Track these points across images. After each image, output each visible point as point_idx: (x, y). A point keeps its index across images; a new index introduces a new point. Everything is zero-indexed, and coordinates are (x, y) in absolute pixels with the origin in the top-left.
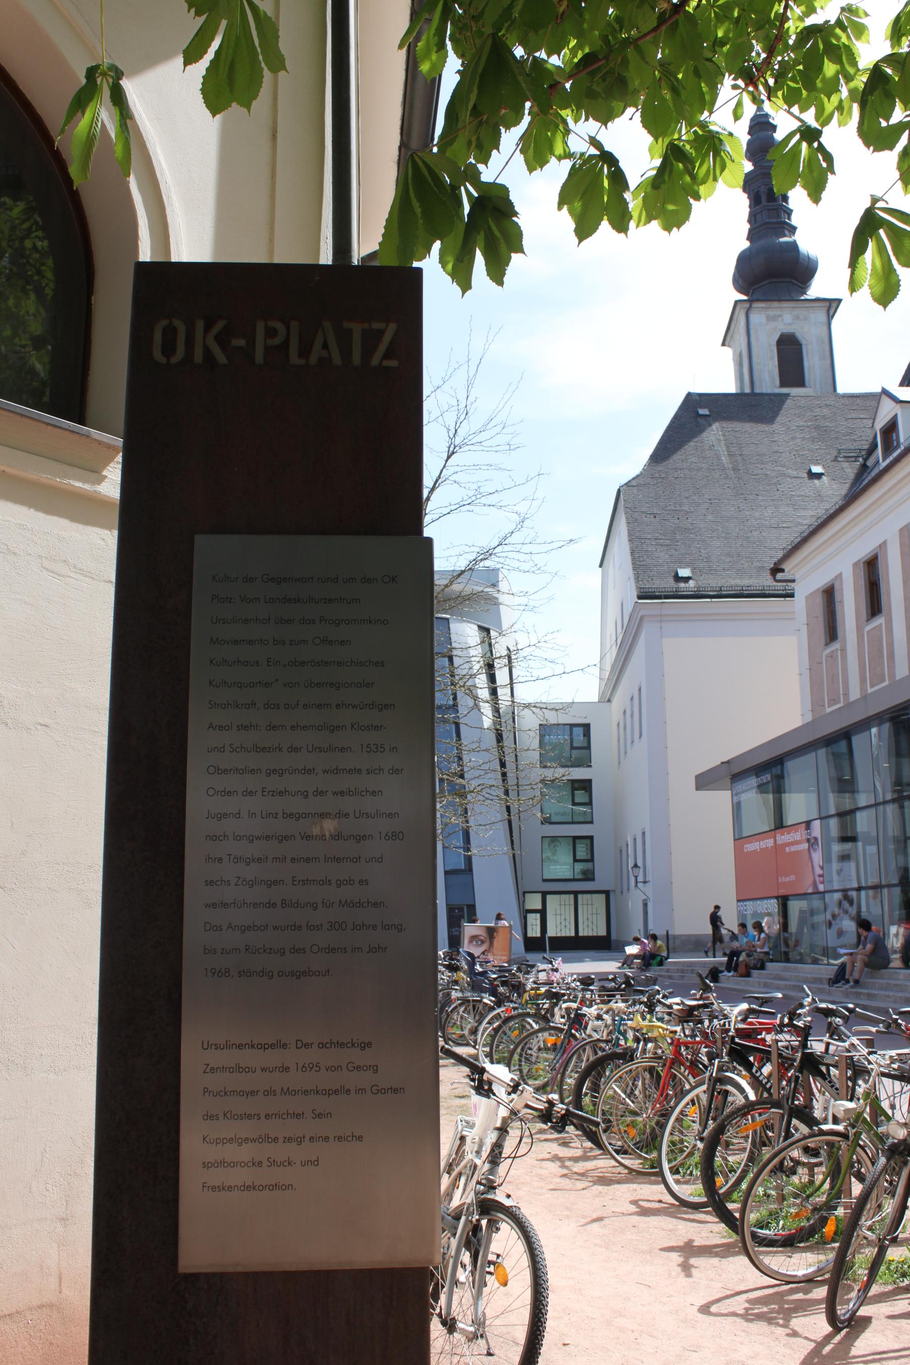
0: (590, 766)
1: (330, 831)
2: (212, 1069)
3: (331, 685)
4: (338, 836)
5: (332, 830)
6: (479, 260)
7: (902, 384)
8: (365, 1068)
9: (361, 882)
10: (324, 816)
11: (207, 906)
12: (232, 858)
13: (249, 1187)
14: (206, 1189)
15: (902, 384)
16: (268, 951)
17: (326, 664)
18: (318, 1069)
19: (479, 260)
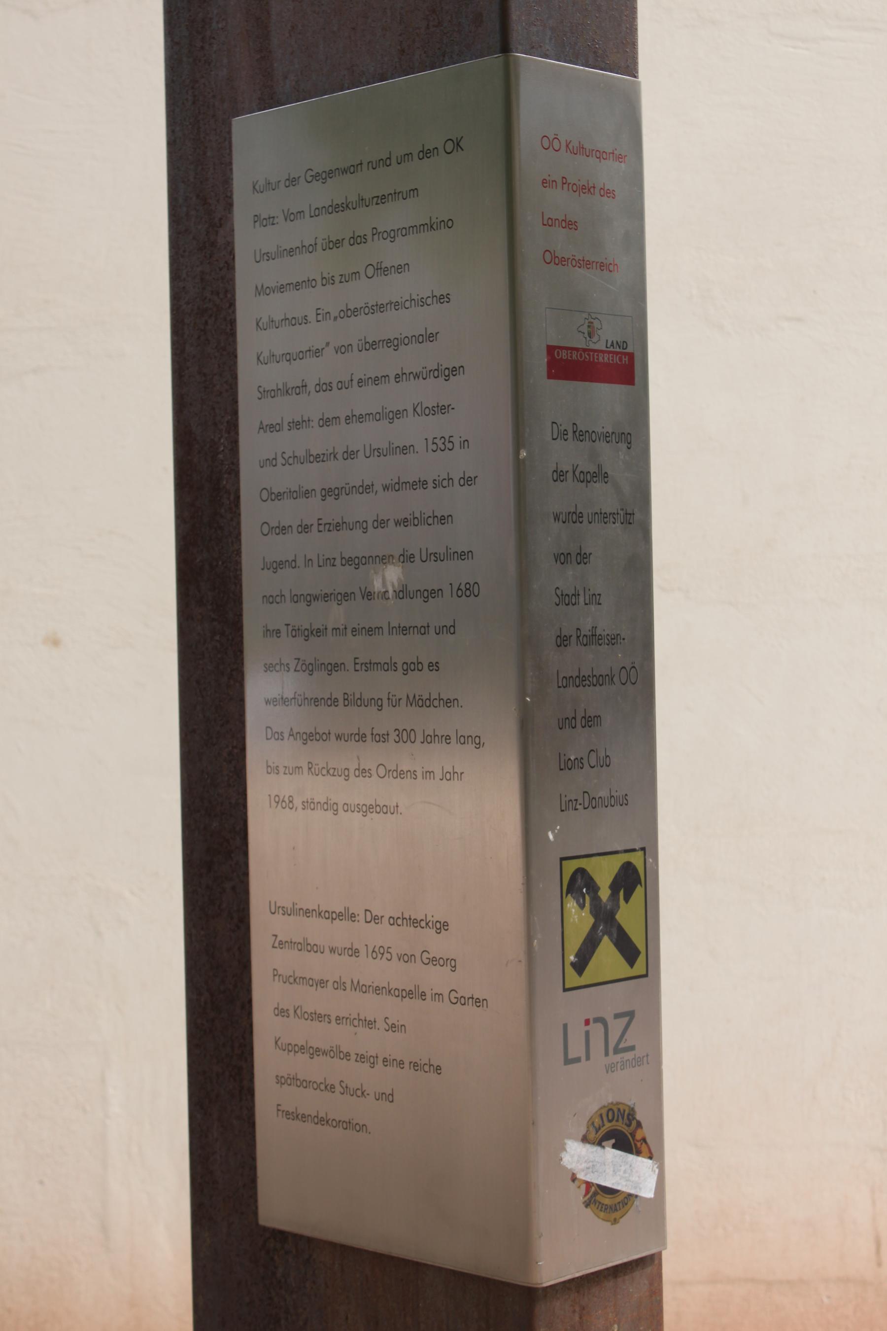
0: (607, 1072)
1: (393, 586)
2: (281, 943)
3: (388, 342)
4: (403, 593)
5: (396, 584)
6: (622, 893)
7: (632, 966)
8: (441, 962)
9: (430, 665)
10: (385, 560)
11: (267, 702)
12: (290, 628)
13: (322, 1119)
14: (280, 1113)
15: (632, 966)
16: (331, 771)
17: (380, 308)
18: (389, 956)
19: (622, 893)
